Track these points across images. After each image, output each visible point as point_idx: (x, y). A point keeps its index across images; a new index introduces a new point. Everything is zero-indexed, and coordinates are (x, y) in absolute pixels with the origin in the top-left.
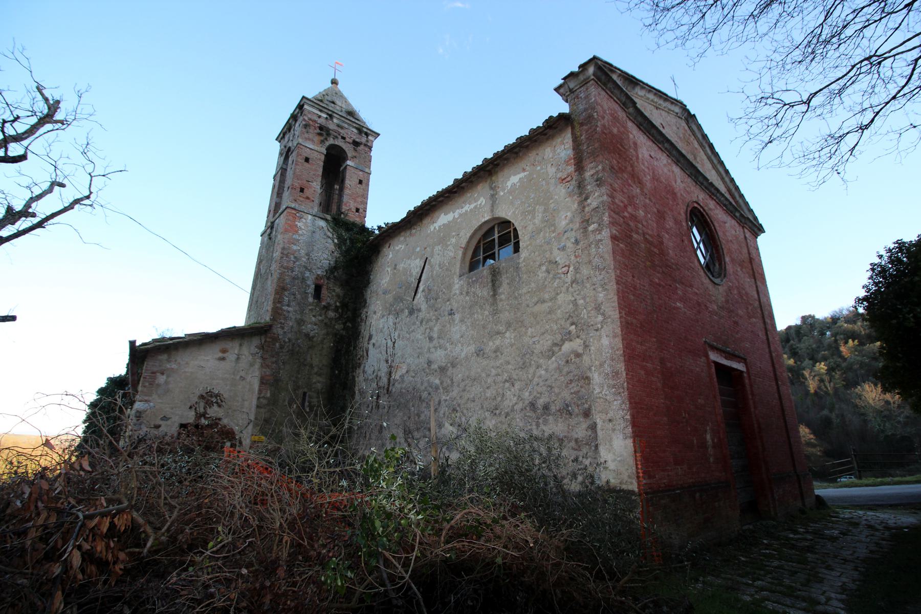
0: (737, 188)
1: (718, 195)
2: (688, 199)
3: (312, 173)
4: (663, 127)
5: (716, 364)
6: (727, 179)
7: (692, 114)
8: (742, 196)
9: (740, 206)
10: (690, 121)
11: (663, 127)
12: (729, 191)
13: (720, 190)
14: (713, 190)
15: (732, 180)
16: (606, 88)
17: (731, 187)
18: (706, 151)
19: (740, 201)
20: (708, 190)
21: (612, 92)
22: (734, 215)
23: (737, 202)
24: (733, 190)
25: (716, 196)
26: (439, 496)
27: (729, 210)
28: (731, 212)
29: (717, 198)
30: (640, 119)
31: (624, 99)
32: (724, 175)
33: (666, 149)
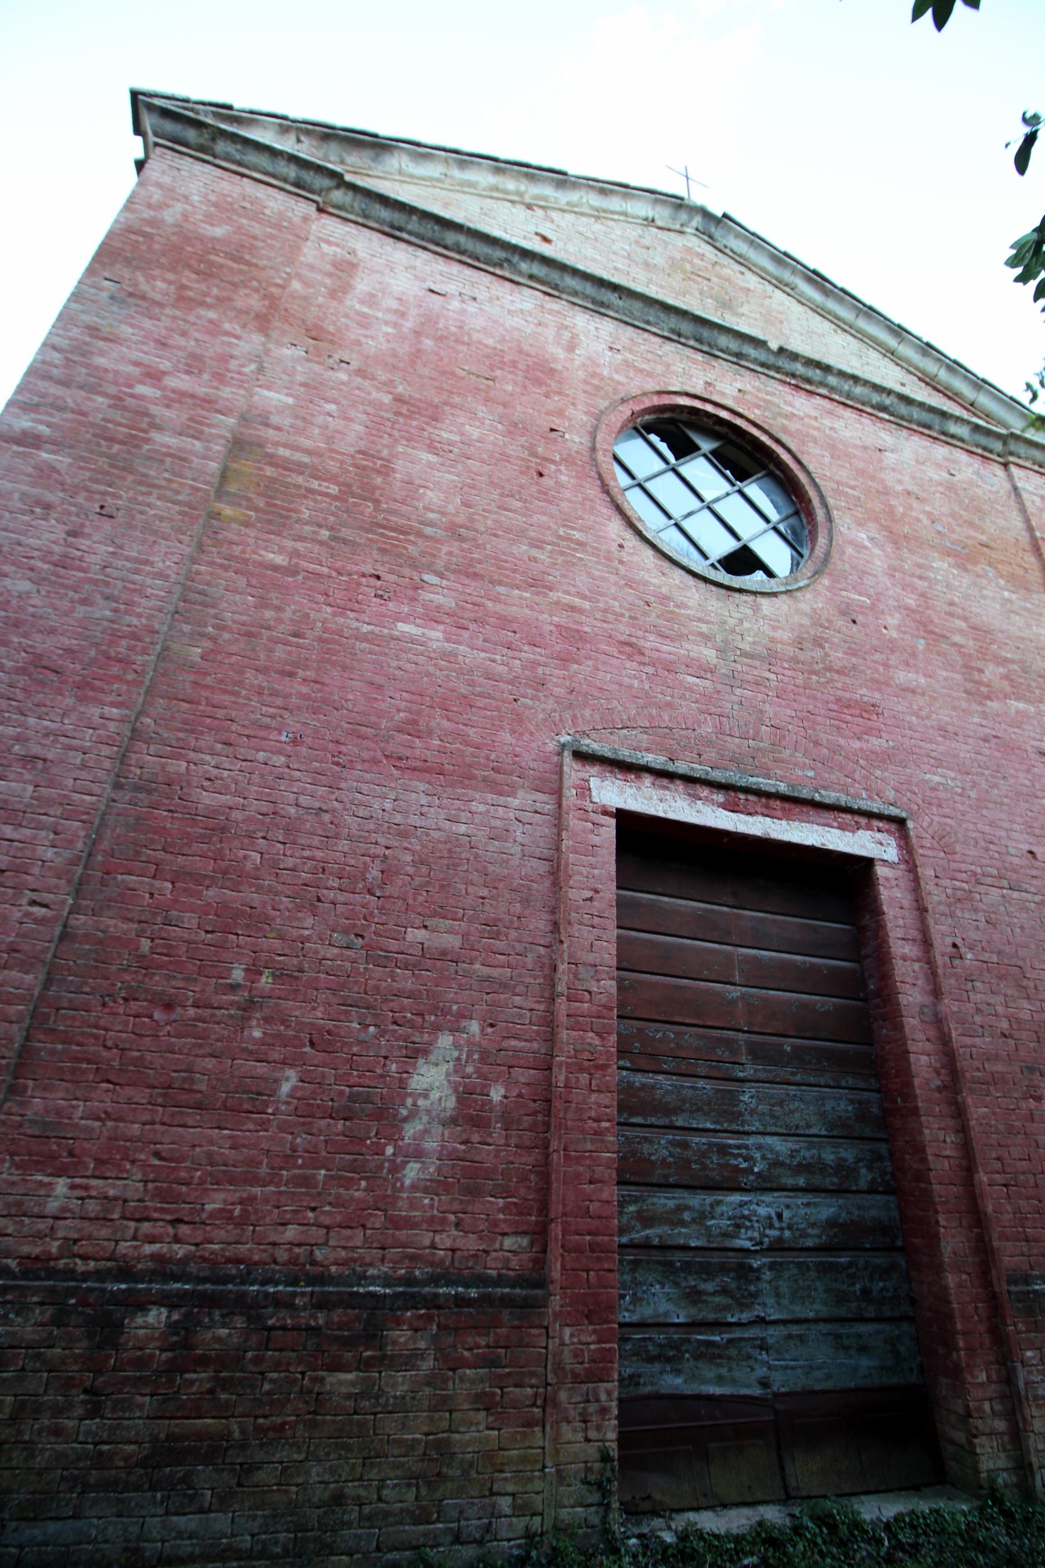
0: (955, 367)
1: (832, 380)
2: (636, 385)
3: (209, 680)
4: (546, 239)
5: (625, 819)
6: (906, 351)
7: (719, 214)
8: (981, 384)
9: (988, 416)
10: (717, 233)
11: (546, 239)
12: (929, 382)
13: (568, 263)
14: (799, 368)
15: (928, 349)
16: (215, 157)
17: (930, 367)
18: (802, 294)
19: (983, 400)
20: (778, 370)
21: (240, 164)
22: (944, 433)
23: (971, 406)
24: (943, 375)
25: (822, 384)
26: (536, 1395)
27: (902, 418)
28: (202, 149)
29: (832, 389)
30: (385, 214)
31: (292, 172)
32: (892, 342)
33: (531, 277)
